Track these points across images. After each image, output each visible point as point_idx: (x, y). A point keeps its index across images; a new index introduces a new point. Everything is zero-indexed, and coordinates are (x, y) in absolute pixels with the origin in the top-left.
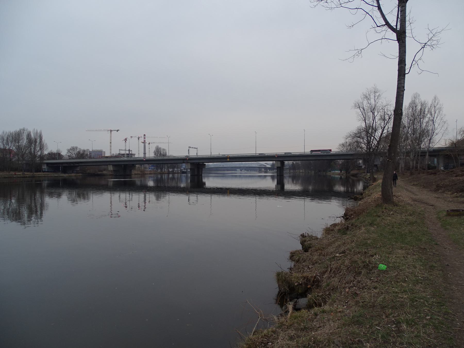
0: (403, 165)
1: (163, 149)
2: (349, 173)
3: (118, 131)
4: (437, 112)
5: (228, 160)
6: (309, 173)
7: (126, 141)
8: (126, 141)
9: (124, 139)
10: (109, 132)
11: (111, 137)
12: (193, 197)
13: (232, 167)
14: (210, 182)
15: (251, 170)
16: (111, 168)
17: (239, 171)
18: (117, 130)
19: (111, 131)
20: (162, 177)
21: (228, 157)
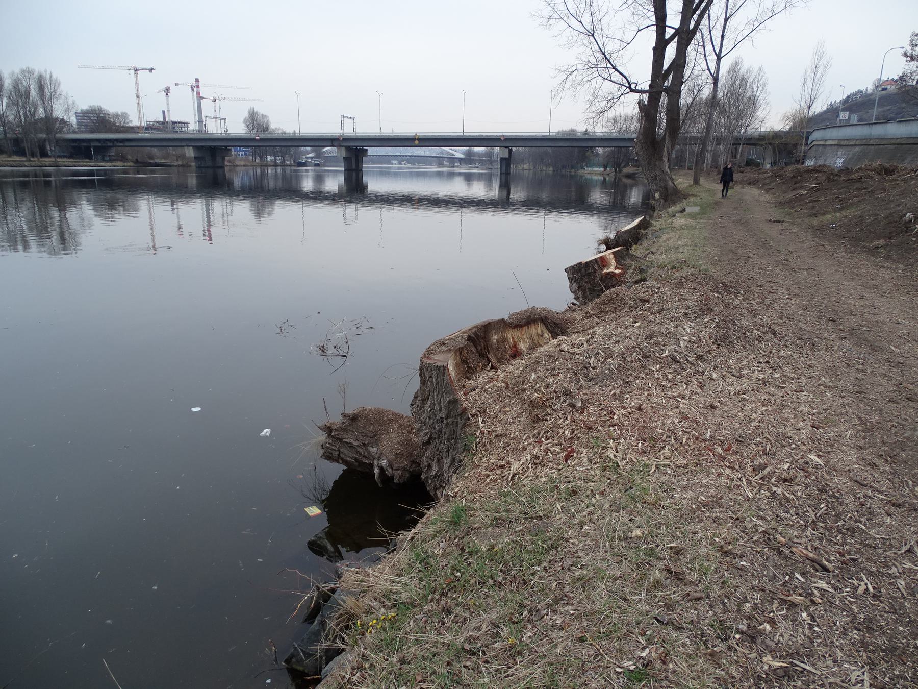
0: (710, 161)
1: (262, 115)
2: (620, 171)
3: (151, 70)
4: (760, 89)
5: (417, 142)
6: (542, 170)
7: (167, 94)
8: (167, 94)
9: (164, 87)
10: (133, 72)
11: (137, 83)
12: (350, 209)
13: (379, 156)
14: (374, 185)
15: (419, 163)
16: (190, 153)
17: (396, 164)
18: (149, 67)
19: (136, 70)
20: (262, 173)
21: (417, 137)
